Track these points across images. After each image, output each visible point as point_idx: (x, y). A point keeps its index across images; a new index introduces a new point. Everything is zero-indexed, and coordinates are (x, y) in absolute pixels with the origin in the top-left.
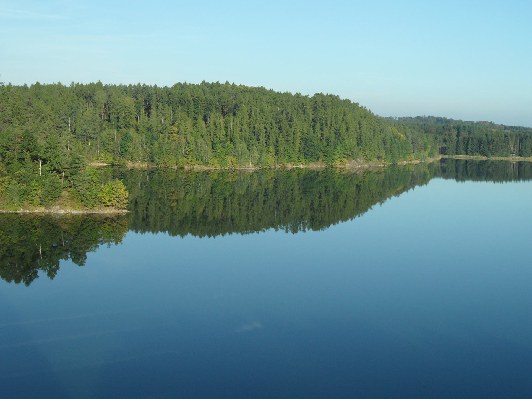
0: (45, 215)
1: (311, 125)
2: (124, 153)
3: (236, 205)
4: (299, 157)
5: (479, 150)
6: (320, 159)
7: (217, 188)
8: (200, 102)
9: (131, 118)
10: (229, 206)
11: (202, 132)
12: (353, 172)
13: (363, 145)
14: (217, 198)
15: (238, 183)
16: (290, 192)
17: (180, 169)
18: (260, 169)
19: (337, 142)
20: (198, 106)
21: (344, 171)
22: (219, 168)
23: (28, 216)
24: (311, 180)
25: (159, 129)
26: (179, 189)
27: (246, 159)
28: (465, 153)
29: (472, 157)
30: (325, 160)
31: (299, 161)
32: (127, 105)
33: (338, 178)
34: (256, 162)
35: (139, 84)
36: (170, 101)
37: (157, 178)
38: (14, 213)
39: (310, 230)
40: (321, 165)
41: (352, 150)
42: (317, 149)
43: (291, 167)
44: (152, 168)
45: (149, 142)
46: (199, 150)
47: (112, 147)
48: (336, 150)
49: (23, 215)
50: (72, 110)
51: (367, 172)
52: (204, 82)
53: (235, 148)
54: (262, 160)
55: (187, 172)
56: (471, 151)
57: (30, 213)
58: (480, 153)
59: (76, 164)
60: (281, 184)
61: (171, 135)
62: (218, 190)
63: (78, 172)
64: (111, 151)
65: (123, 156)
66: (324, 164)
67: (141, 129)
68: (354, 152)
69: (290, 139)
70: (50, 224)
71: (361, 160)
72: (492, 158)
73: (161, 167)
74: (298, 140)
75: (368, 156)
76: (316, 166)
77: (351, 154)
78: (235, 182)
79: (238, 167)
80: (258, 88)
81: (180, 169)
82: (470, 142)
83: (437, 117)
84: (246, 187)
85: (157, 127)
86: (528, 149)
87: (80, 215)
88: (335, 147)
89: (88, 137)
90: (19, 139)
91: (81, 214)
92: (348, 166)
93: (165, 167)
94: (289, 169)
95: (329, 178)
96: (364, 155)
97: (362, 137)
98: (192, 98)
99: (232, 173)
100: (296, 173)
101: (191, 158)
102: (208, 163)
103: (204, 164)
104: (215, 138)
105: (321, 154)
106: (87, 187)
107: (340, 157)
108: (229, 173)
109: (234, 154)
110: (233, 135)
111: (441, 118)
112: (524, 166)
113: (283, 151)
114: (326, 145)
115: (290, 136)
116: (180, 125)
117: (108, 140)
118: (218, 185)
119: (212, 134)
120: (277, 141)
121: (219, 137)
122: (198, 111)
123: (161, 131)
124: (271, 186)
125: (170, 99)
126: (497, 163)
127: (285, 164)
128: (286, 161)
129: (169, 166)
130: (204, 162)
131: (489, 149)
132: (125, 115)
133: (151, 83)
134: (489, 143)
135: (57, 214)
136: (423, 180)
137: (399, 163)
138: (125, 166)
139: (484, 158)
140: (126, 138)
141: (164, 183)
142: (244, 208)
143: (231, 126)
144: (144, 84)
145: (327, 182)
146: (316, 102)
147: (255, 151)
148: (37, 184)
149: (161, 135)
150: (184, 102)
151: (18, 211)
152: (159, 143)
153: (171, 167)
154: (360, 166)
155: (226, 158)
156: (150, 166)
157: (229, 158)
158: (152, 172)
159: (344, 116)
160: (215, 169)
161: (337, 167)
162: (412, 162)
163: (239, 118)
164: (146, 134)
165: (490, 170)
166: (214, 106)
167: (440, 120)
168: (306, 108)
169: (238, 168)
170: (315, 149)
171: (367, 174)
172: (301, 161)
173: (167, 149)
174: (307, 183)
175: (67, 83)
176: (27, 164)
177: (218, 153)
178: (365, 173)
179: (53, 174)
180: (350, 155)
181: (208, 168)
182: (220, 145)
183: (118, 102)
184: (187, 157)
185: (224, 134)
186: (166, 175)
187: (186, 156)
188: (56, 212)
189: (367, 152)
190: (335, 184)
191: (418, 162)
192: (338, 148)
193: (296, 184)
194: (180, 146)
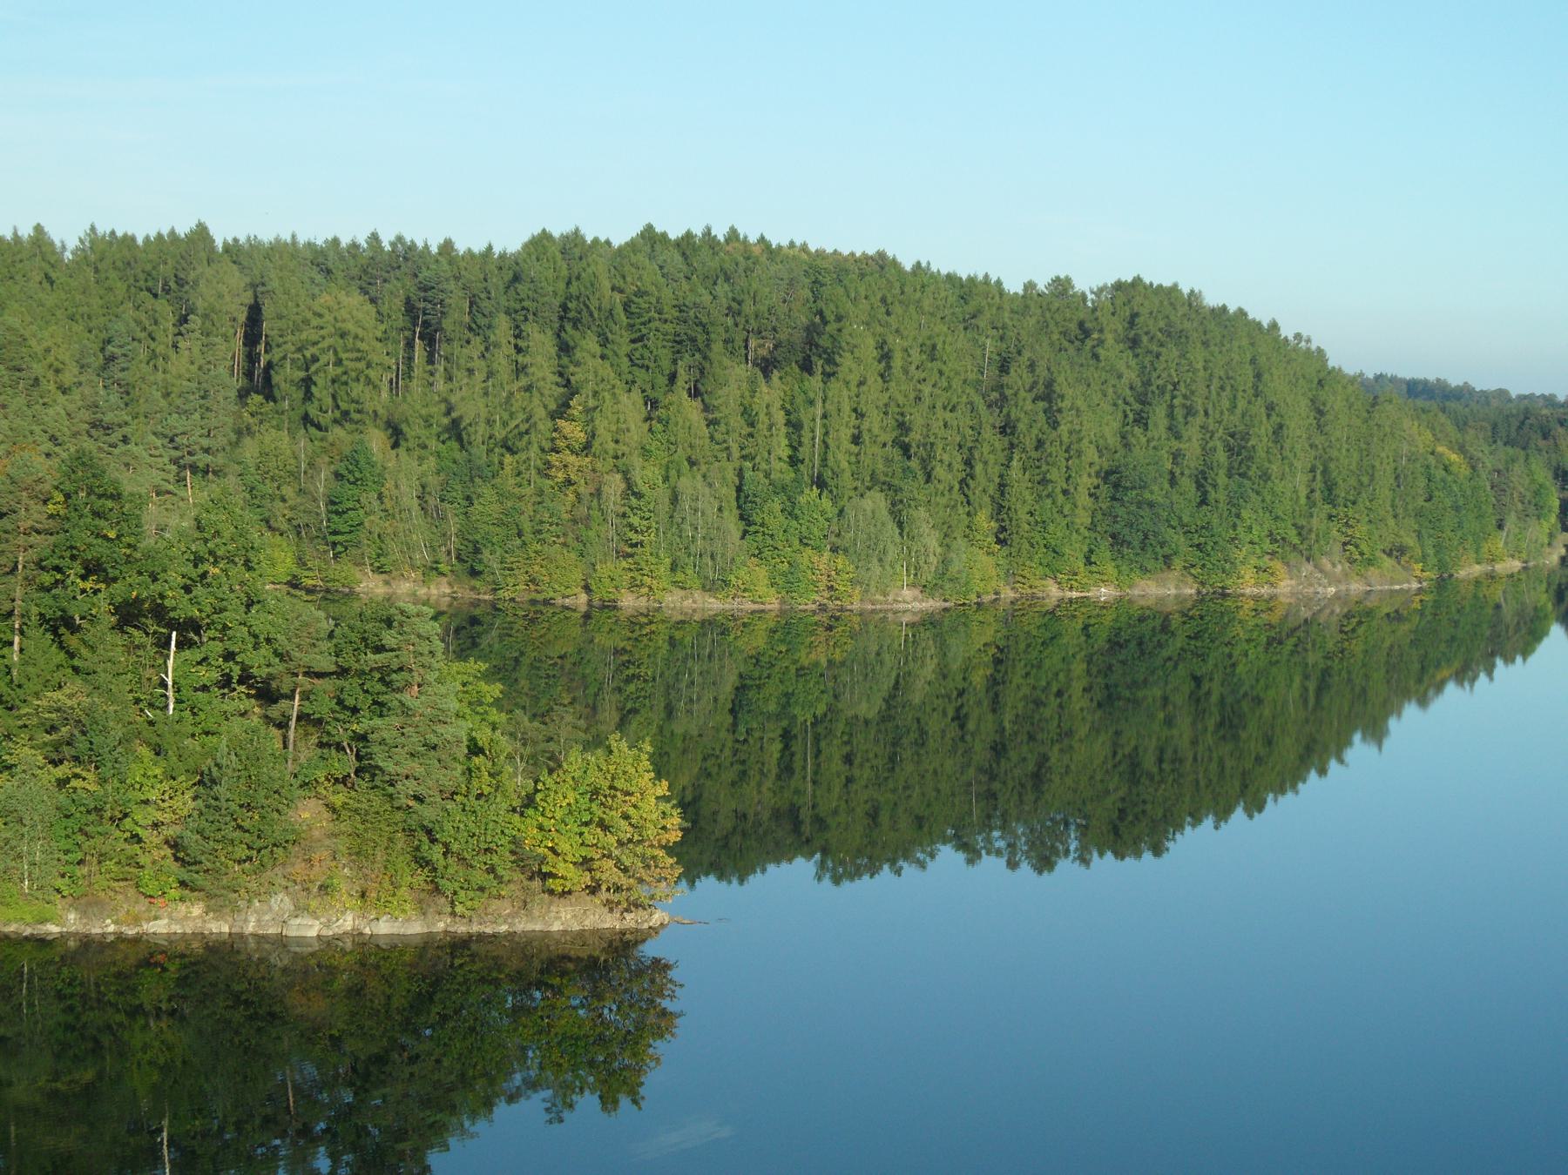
0: (207, 948)
1: (1126, 416)
2: (348, 537)
3: (837, 765)
4: (1091, 551)
6: (1178, 563)
7: (766, 692)
8: (653, 314)
9: (369, 381)
10: (804, 768)
11: (691, 446)
12: (1305, 613)
13: (1340, 501)
14: (757, 735)
15: (852, 670)
16: (1054, 702)
17: (603, 607)
18: (946, 610)
19: (1240, 486)
20: (644, 331)
21: (1270, 609)
22: (773, 603)
23: (109, 952)
24: (1143, 653)
25: (500, 433)
26: (596, 695)
27: (888, 567)
30: (1193, 566)
31: (1094, 568)
32: (350, 326)
33: (1248, 641)
34: (928, 575)
35: (374, 237)
36: (523, 308)
37: (496, 646)
38: (26, 938)
39: (1105, 858)
40: (1177, 587)
41: (1302, 522)
42: (1167, 521)
44: (476, 604)
45: (458, 487)
46: (686, 527)
47: (292, 508)
48: (1238, 522)
49: (76, 952)
50: (110, 348)
51: (1357, 616)
52: (649, 228)
53: (841, 512)
54: (954, 569)
55: (633, 623)
57: (120, 938)
59: (379, 649)
60: (1020, 670)
61: (553, 458)
62: (766, 700)
63: (391, 699)
64: (284, 526)
65: (340, 548)
66: (1190, 580)
67: (413, 431)
68: (1310, 530)
69: (1054, 475)
70: (237, 1000)
71: (1334, 565)
73: (512, 600)
74: (1086, 481)
75: (1364, 547)
76: (1161, 592)
77: (1296, 541)
78: (843, 664)
79: (856, 600)
80: (865, 257)
81: (603, 607)
83: (1408, 376)
84: (887, 684)
85: (490, 423)
87: (406, 946)
88: (1233, 510)
89: (184, 467)
90: (40, 507)
91: (417, 941)
93: (533, 602)
94: (1050, 603)
95: (1212, 641)
96: (1345, 544)
97: (1332, 466)
98: (618, 297)
99: (830, 628)
101: (653, 560)
102: (726, 583)
103: (709, 587)
104: (748, 474)
105: (1178, 540)
106: (449, 785)
107: (1258, 551)
108: (816, 624)
109: (838, 542)
110: (824, 460)
111: (1425, 382)
113: (1027, 527)
114: (1198, 500)
115: (1053, 464)
116: (597, 414)
117: (273, 479)
118: (769, 677)
119: (736, 453)
120: (1002, 487)
121: (764, 466)
122: (647, 354)
123: (505, 439)
124: (978, 678)
125: (521, 300)
127: (1037, 583)
128: (1040, 571)
129: (552, 594)
130: (706, 578)
132: (339, 370)
133: (426, 234)
135: (281, 942)
137: (1462, 574)
138: (351, 595)
140: (352, 471)
141: (524, 670)
142: (864, 774)
143: (814, 420)
144: (400, 239)
145: (1203, 657)
146: (1134, 316)
147: (925, 528)
148: (158, 771)
149: (508, 459)
150: (585, 313)
151: (53, 929)
152: (502, 495)
153: (559, 601)
154: (1331, 590)
155: (806, 561)
156: (465, 594)
157: (815, 559)
158: (474, 621)
159: (1258, 376)
160: (756, 607)
161: (1243, 595)
162: (1499, 567)
163: (847, 383)
164: (438, 454)
166: (718, 335)
167: (1420, 388)
168: (1101, 342)
169: (856, 606)
170: (1158, 516)
171: (1360, 623)
172: (1101, 568)
173: (542, 522)
174: (1123, 663)
175: (67, 235)
176: (92, 648)
177: (769, 541)
178: (1348, 616)
179: (229, 706)
181: (727, 606)
182: (776, 505)
183: (309, 315)
184: (631, 556)
185: (785, 452)
186: (536, 635)
187: (629, 550)
188: (272, 931)
189: (1361, 530)
190: (1234, 665)
191: (1516, 565)
192: (1245, 514)
193: (1079, 668)
194: (601, 510)
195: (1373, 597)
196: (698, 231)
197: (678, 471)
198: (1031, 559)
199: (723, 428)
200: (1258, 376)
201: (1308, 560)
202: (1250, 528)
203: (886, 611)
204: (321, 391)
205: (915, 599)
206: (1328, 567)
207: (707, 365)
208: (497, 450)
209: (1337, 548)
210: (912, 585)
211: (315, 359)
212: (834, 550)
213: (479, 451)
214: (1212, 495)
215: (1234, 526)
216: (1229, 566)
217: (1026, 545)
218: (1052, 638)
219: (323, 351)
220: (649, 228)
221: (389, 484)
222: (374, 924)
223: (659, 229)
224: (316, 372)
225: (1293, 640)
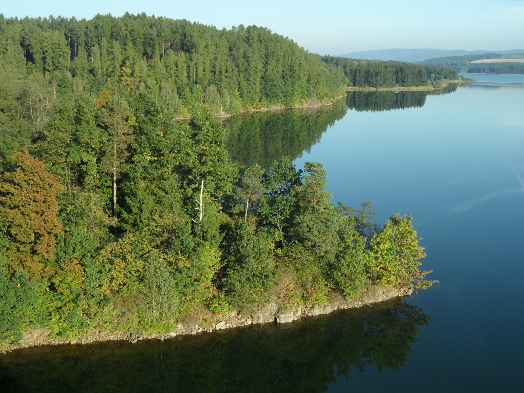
4: (261, 99)
5: (367, 81)
12: (310, 112)
28: (352, 84)
29: (361, 88)
31: (262, 103)
33: (297, 120)
34: (227, 107)
36: (101, 36)
40: (280, 107)
43: (254, 110)
56: (359, 83)
58: (368, 84)
61: (122, 78)
69: (251, 78)
72: (380, 89)
77: (307, 94)
82: (358, 74)
86: (410, 80)
92: (306, 107)
94: (252, 113)
100: (258, 118)
112: (406, 95)
121: (181, 79)
126: (385, 94)
131: (376, 81)
133: (67, 15)
134: (376, 75)
139: (374, 89)
145: (287, 125)
146: (259, 35)
149: (109, 79)
150: (118, 36)
165: (378, 100)
180: (307, 95)
185: (186, 75)
193: (258, 130)
195: (323, 107)
196: (14, 18)
197: (160, 81)
198: (247, 101)
199: (169, 68)
200: (293, 52)
201: (310, 98)
202: (297, 91)
203: (218, 118)
204: (49, 60)
205: (225, 114)
206: (314, 100)
207: (154, 50)
208: (105, 76)
209: (315, 95)
210: (223, 110)
211: (47, 51)
212: (204, 102)
213: (99, 76)
214: (287, 82)
215: (293, 90)
216: (293, 101)
217: (246, 98)
218: (252, 123)
219: (49, 49)
220: (98, 14)
221: (75, 87)
222: (312, 310)
223: (130, 14)
224: (47, 55)
225: (306, 120)
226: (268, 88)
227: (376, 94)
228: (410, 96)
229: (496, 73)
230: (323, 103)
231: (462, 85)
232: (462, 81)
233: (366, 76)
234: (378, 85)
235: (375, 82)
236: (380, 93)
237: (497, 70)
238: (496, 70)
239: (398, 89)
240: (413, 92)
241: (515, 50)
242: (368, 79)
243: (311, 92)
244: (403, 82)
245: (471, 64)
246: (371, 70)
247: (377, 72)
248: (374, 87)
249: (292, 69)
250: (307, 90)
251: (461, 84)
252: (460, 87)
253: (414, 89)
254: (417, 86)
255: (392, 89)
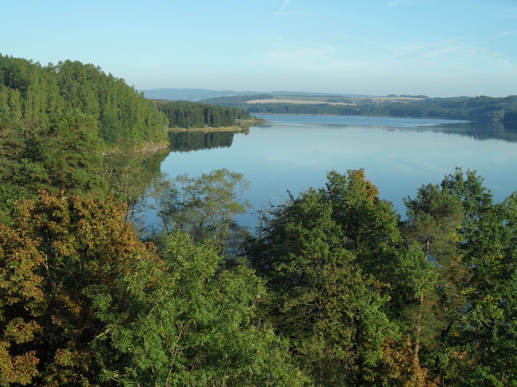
5: (177, 121)
29: (171, 129)
58: (178, 125)
72: (191, 130)
77: (145, 136)
86: (218, 121)
112: (216, 135)
134: (186, 115)
136: (166, 154)
139: (184, 130)
165: (188, 141)
195: (160, 151)
201: (147, 141)
215: (131, 133)
226: (107, 130)
227: (186, 135)
228: (219, 136)
229: (273, 113)
230: (160, 146)
231: (255, 125)
232: (255, 121)
233: (175, 117)
234: (189, 125)
235: (185, 122)
236: (191, 134)
237: (274, 110)
238: (272, 110)
239: (207, 129)
240: (222, 132)
241: (301, 92)
242: (177, 119)
243: (149, 135)
244: (212, 122)
245: (247, 104)
246: (181, 111)
247: (187, 112)
248: (184, 127)
249: (128, 110)
250: (145, 133)
251: (254, 124)
252: (252, 127)
253: (223, 129)
254: (225, 126)
255: (203, 129)
